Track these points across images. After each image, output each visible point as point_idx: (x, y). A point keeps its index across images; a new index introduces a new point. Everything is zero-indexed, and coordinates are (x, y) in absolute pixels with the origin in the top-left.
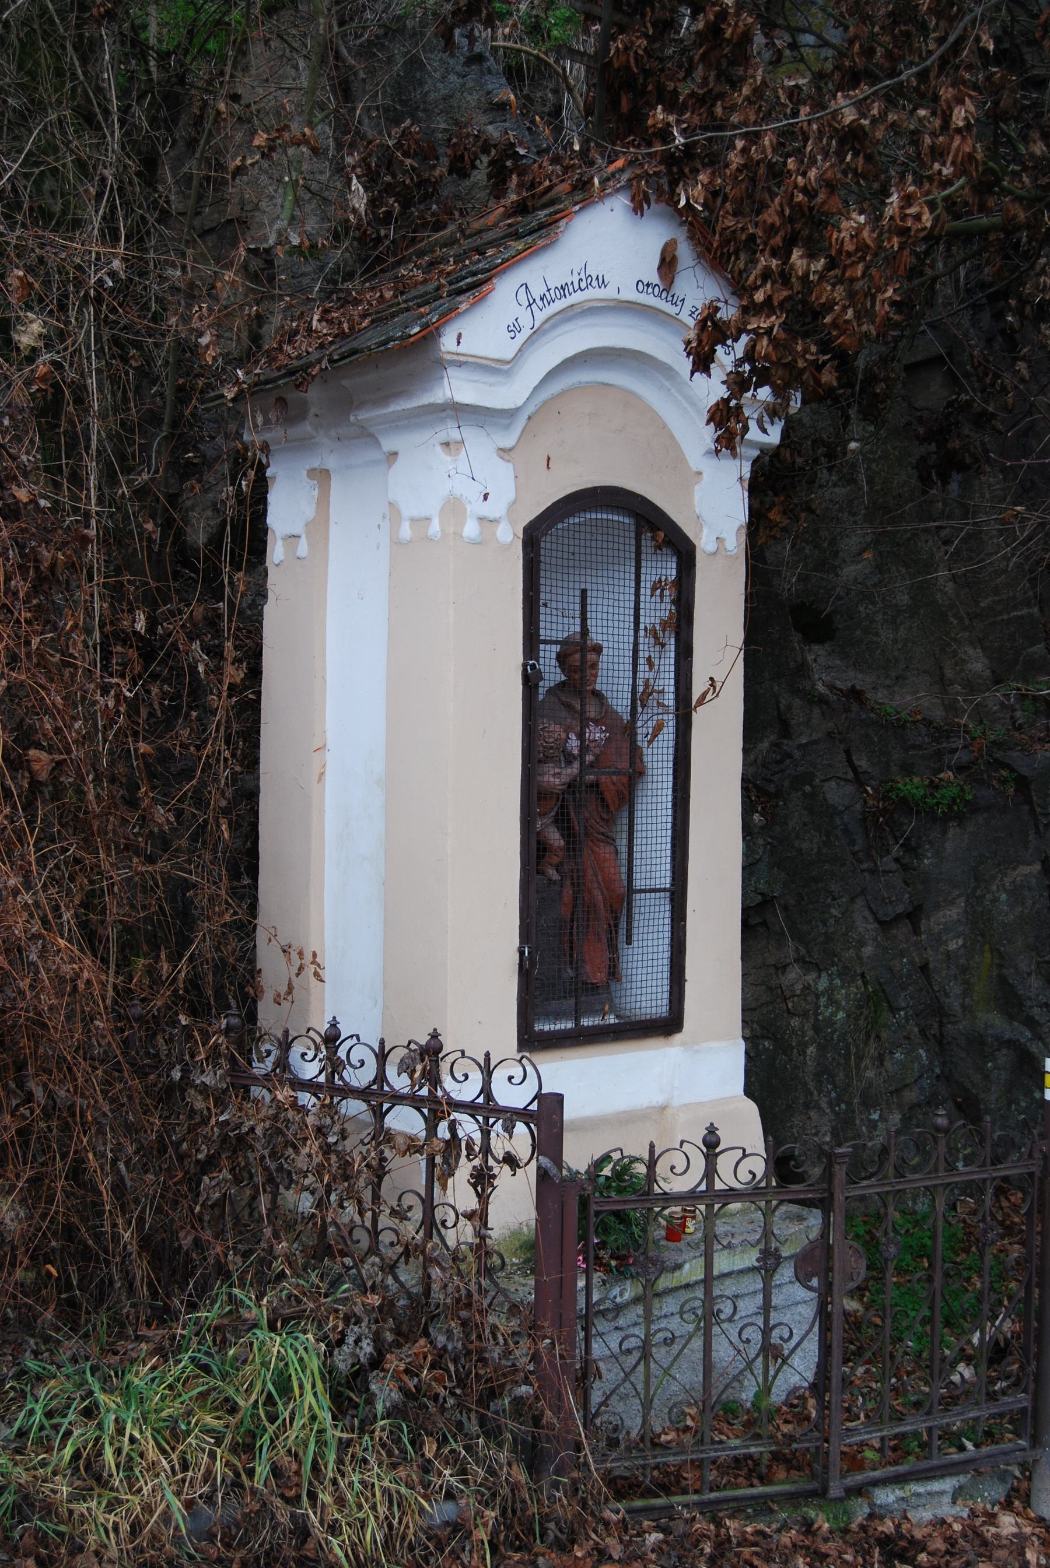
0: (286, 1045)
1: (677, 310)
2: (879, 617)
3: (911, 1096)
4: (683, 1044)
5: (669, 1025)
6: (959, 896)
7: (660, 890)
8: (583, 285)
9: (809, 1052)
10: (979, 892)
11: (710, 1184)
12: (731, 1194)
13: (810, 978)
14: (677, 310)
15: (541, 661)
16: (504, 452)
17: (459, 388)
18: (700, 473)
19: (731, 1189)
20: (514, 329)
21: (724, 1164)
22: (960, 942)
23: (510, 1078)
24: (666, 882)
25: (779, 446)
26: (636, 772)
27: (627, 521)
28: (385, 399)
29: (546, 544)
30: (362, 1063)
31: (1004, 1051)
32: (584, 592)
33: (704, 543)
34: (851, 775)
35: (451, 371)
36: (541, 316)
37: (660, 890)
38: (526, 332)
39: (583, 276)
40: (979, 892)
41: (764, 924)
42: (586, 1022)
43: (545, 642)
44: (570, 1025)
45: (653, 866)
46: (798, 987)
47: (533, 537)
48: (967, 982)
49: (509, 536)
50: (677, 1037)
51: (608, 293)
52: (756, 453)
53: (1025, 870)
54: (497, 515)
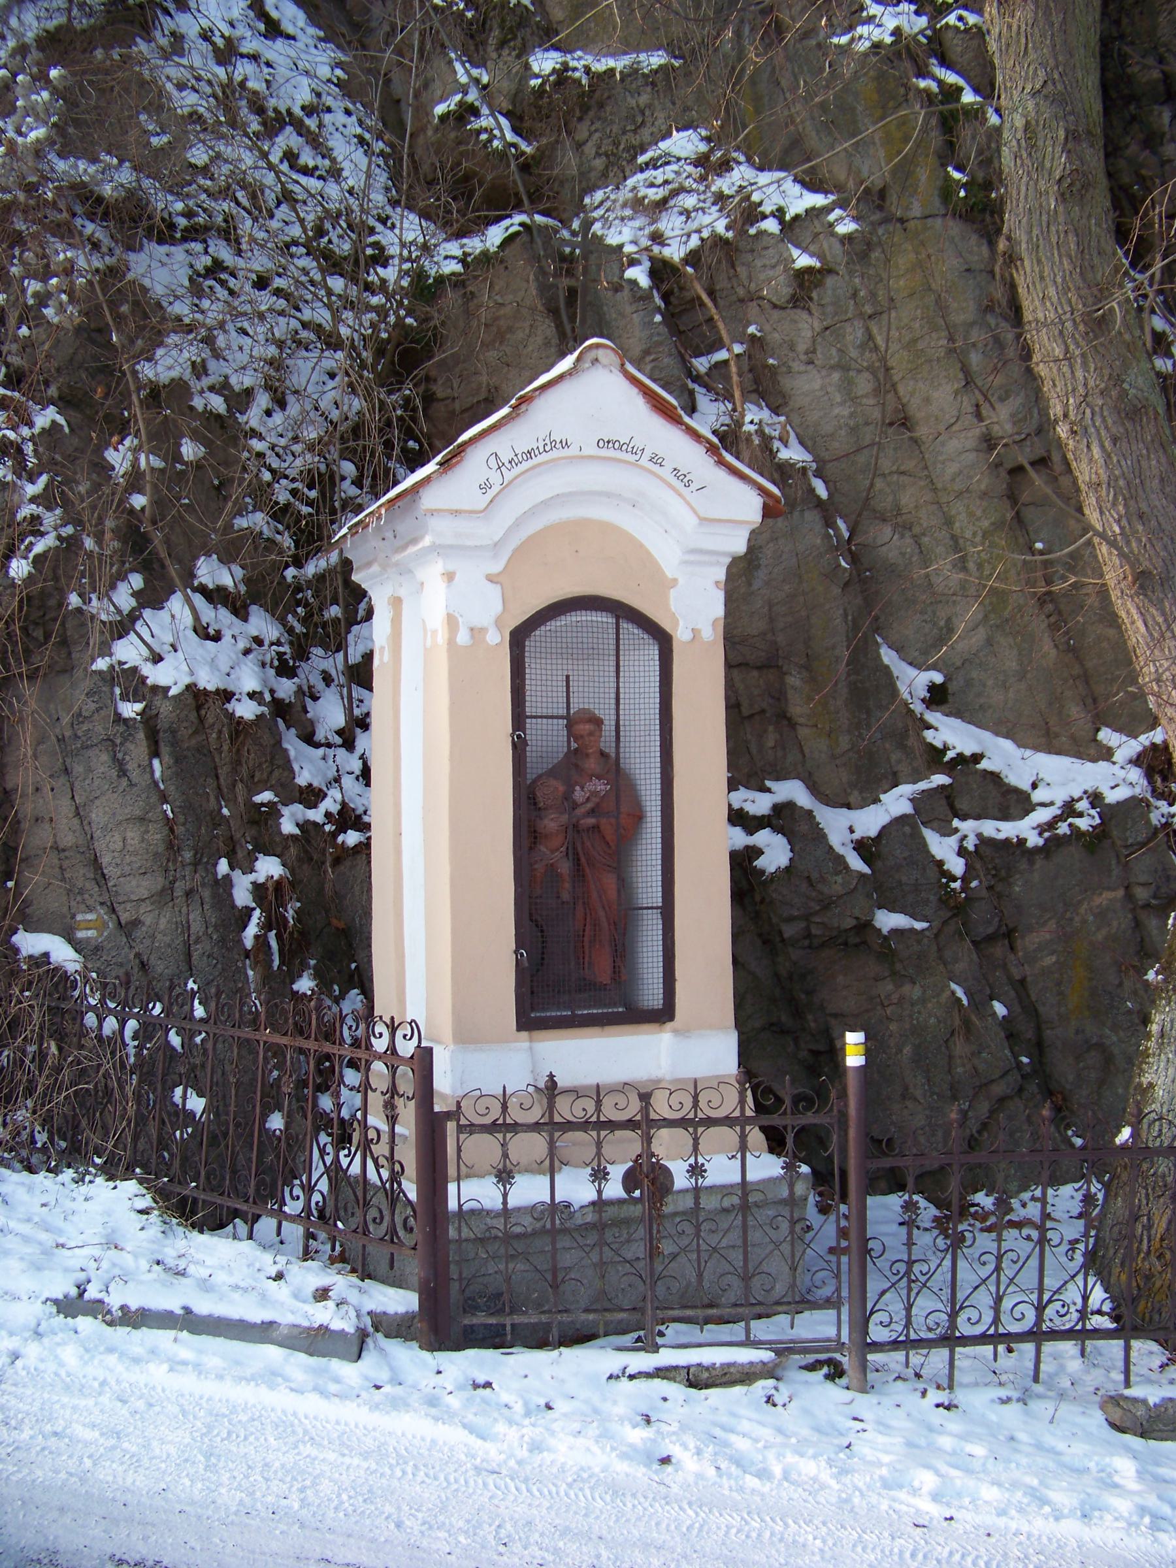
0: (393, 1028)
2: (990, 683)
3: (998, 1089)
4: (675, 1031)
5: (664, 1014)
10: (1068, 915)
16: (490, 579)
17: (437, 531)
19: (569, 1122)
20: (485, 487)
22: (1054, 959)
23: (405, 1036)
24: (659, 902)
26: (638, 817)
30: (381, 1035)
31: (1093, 1053)
32: (568, 677)
36: (509, 476)
38: (496, 489)
40: (1068, 915)
41: (864, 943)
43: (532, 717)
45: (649, 891)
46: (895, 998)
47: (519, 638)
48: (1060, 993)
49: (498, 639)
50: (669, 1025)
51: (573, 451)
52: (728, 560)
53: (1108, 895)
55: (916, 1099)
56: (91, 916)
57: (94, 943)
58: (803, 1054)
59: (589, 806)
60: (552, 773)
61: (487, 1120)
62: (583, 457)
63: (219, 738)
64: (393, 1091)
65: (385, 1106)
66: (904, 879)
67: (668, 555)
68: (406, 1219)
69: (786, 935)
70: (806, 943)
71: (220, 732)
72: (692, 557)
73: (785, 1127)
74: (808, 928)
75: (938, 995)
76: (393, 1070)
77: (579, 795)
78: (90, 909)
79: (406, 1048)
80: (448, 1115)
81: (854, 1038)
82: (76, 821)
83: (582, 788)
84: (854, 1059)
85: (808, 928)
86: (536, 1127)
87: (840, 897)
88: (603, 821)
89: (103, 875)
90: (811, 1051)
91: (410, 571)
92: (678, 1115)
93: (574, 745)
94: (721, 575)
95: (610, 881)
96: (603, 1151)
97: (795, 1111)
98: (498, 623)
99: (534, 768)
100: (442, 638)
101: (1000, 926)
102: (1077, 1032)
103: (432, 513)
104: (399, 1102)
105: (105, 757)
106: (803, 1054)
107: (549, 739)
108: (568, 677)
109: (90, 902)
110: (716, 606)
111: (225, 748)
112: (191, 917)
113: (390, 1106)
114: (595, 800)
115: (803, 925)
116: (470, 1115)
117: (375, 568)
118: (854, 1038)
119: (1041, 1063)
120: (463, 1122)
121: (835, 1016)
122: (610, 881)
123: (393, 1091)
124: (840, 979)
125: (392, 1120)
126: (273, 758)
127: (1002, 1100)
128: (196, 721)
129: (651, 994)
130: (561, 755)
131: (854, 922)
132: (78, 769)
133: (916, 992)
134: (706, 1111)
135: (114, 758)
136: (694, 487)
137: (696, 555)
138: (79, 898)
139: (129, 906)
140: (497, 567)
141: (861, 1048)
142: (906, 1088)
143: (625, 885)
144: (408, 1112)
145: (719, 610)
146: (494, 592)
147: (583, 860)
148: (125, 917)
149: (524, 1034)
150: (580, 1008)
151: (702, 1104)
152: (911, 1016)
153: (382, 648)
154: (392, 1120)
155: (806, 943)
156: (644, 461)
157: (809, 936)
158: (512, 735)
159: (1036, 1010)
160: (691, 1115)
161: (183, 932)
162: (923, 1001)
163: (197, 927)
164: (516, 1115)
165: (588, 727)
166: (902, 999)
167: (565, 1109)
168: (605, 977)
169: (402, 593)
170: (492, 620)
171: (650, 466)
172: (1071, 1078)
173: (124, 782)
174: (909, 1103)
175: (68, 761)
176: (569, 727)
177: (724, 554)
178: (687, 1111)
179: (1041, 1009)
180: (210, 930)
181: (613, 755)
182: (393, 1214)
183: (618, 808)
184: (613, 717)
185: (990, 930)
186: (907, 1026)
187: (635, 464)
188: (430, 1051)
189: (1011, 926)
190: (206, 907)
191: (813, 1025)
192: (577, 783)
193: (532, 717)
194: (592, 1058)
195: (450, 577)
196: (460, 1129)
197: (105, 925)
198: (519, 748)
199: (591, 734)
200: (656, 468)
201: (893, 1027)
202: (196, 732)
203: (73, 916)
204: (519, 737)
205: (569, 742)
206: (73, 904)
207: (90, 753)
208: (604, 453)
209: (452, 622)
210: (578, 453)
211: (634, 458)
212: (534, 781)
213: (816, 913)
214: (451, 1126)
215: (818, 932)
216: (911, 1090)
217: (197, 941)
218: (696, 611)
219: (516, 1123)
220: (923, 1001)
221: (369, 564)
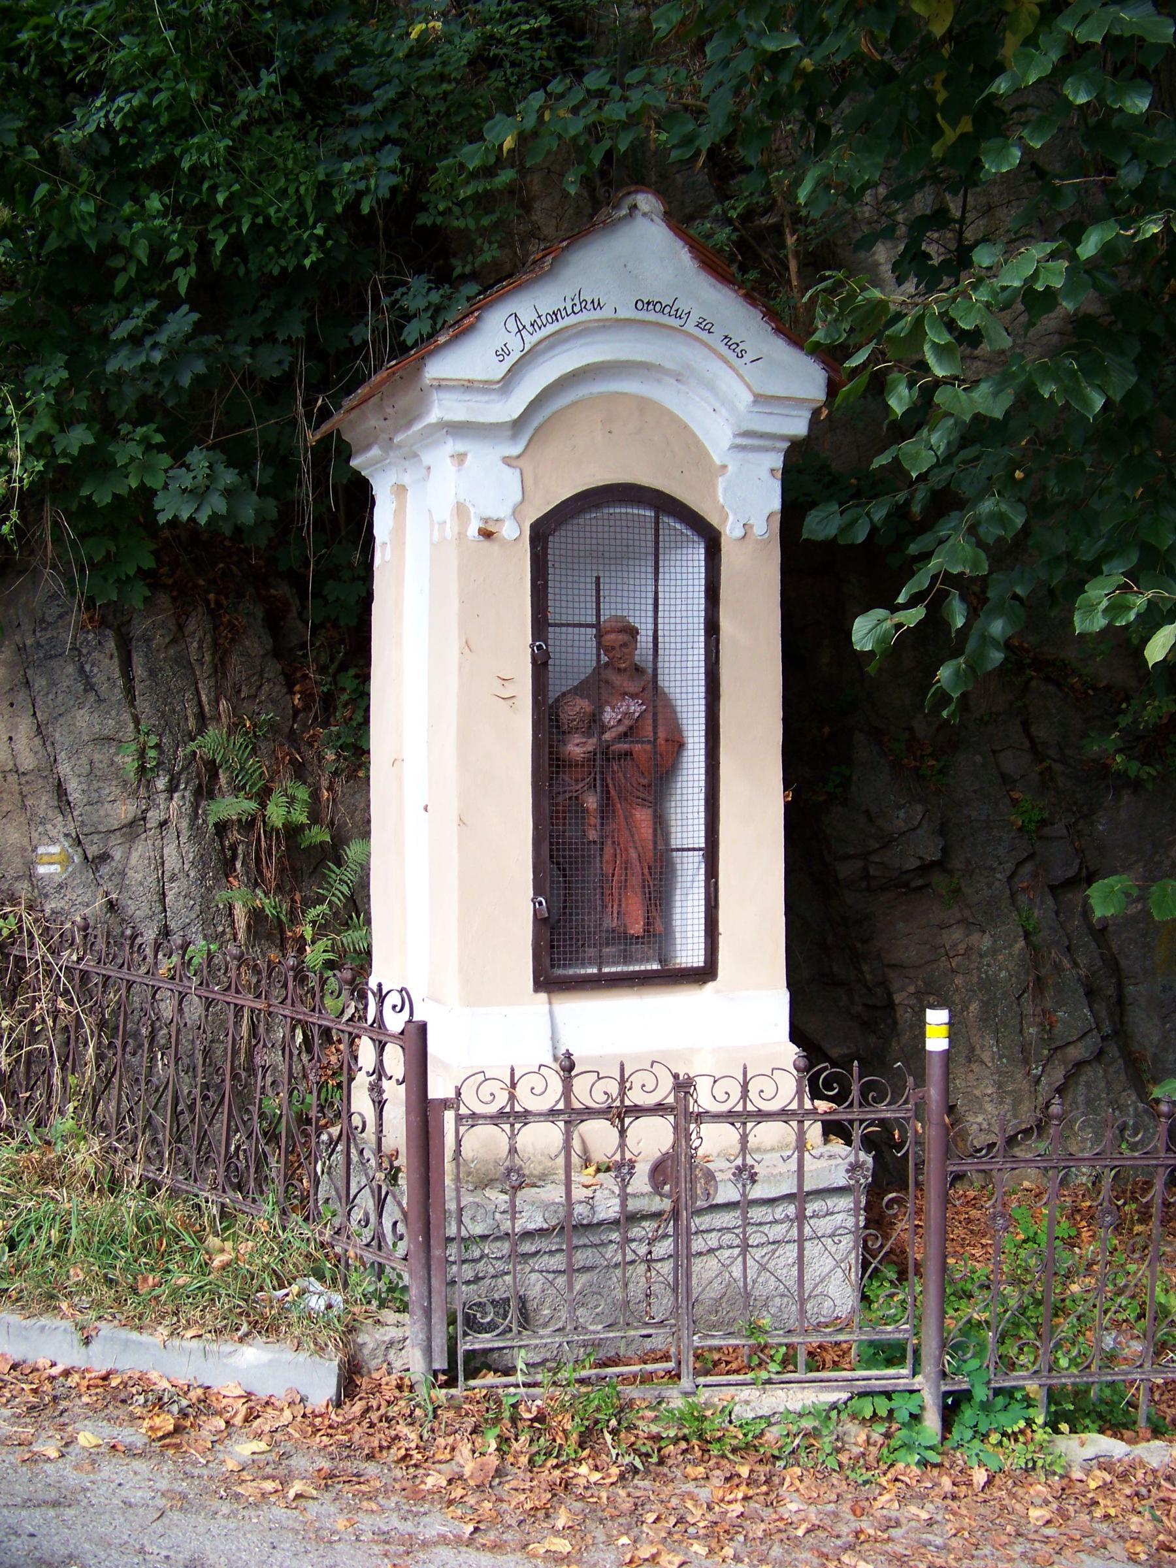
1: (682, 322)
3: (1075, 1053)
4: (717, 992)
5: (706, 973)
6: (1136, 862)
7: (694, 849)
8: (576, 309)
9: (972, 1008)
10: (1157, 858)
11: (568, 1101)
12: (589, 1113)
13: (975, 937)
14: (682, 322)
15: (550, 642)
16: (507, 461)
17: (443, 408)
18: (724, 467)
21: (581, 1086)
25: (809, 436)
26: (678, 745)
27: (648, 513)
28: (409, 424)
29: (555, 545)
32: (598, 578)
33: (730, 531)
34: (1027, 744)
35: (435, 396)
36: (530, 340)
37: (694, 849)
38: (515, 356)
39: (577, 301)
40: (1157, 858)
42: (606, 970)
43: (555, 625)
44: (595, 971)
45: (688, 828)
46: (961, 948)
47: (542, 534)
50: (710, 986)
51: (606, 313)
52: (786, 445)
54: (502, 516)
55: (982, 1062)
56: (55, 849)
57: (57, 879)
58: (857, 1009)
59: (621, 729)
60: (580, 690)
61: (493, 1109)
62: (618, 320)
63: (200, 648)
64: (379, 1071)
65: (371, 1090)
66: (974, 814)
67: (716, 433)
68: (395, 1224)
69: (841, 876)
70: (864, 884)
71: (201, 641)
72: (739, 441)
73: (851, 1122)
74: (865, 869)
75: (1011, 946)
76: (381, 1047)
77: (609, 716)
78: (53, 841)
79: (395, 1022)
80: (445, 1104)
81: (937, 1019)
82: (37, 741)
83: (613, 708)
84: (936, 1040)
85: (865, 869)
86: (552, 1114)
87: (902, 834)
88: (638, 747)
89: (69, 803)
90: (865, 1005)
91: (415, 455)
92: (724, 1108)
93: (604, 659)
94: (776, 461)
95: (643, 816)
96: (628, 1141)
97: (864, 1101)
98: (516, 513)
99: (557, 686)
100: (450, 532)
101: (1080, 869)
102: (1164, 989)
103: (441, 386)
104: (385, 1083)
105: (70, 669)
106: (857, 1009)
107: (578, 653)
108: (598, 578)
109: (53, 833)
110: (768, 498)
111: (207, 658)
112: (166, 851)
113: (376, 1089)
114: (627, 722)
115: (860, 864)
116: (471, 1103)
117: (375, 452)
118: (937, 1019)
119: (1122, 1023)
120: (463, 1111)
121: (893, 966)
122: (643, 816)
123: (379, 1071)
124: (900, 925)
125: (380, 1105)
126: (262, 672)
127: (1079, 1065)
128: (174, 628)
129: (689, 951)
130: (589, 671)
131: (918, 863)
132: (40, 683)
133: (986, 942)
134: (757, 1102)
135: (81, 670)
136: (748, 358)
137: (750, 440)
138: (41, 829)
139: (96, 838)
140: (515, 450)
141: (945, 1029)
142: (972, 1049)
143: (661, 824)
144: (396, 1094)
145: (776, 504)
146: (511, 477)
147: (613, 792)
148: (92, 851)
149: (543, 996)
150: (608, 964)
151: (753, 1094)
152: (979, 969)
153: (385, 544)
154: (380, 1105)
155: (864, 884)
156: (690, 327)
157: (866, 876)
158: (532, 646)
159: (1117, 964)
160: (739, 1108)
161: (156, 868)
162: (994, 952)
163: (172, 862)
164: (526, 1101)
165: (623, 637)
166: (969, 949)
167: (585, 1093)
168: (637, 928)
169: (406, 479)
170: (510, 512)
171: (697, 332)
172: (1156, 1039)
173: (92, 697)
174: (974, 1066)
175: (30, 672)
176: (599, 637)
177: (782, 438)
178: (733, 1102)
179: (1124, 963)
180: (186, 867)
181: (650, 671)
182: (380, 1216)
183: (655, 733)
184: (651, 626)
185: (1071, 873)
186: (975, 980)
187: (679, 330)
188: (423, 1028)
189: (1092, 869)
190: (183, 840)
191: (868, 977)
192: (608, 703)
193: (555, 625)
194: (616, 1028)
195: (460, 458)
196: (459, 1118)
197: (70, 858)
198: (541, 665)
199: (625, 645)
200: (704, 335)
201: (959, 980)
202: (174, 641)
203: (34, 849)
204: (539, 647)
205: (598, 655)
206: (35, 835)
207: (54, 664)
208: (642, 315)
209: (461, 510)
210: (611, 315)
211: (676, 323)
212: (557, 700)
213: (875, 851)
214: (449, 1116)
215: (877, 874)
216: (978, 1052)
217: (173, 879)
218: (747, 501)
219: (526, 1111)
220: (994, 952)
221: (368, 447)
